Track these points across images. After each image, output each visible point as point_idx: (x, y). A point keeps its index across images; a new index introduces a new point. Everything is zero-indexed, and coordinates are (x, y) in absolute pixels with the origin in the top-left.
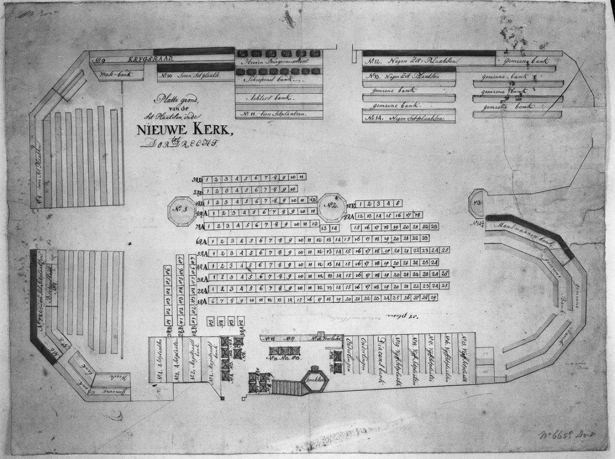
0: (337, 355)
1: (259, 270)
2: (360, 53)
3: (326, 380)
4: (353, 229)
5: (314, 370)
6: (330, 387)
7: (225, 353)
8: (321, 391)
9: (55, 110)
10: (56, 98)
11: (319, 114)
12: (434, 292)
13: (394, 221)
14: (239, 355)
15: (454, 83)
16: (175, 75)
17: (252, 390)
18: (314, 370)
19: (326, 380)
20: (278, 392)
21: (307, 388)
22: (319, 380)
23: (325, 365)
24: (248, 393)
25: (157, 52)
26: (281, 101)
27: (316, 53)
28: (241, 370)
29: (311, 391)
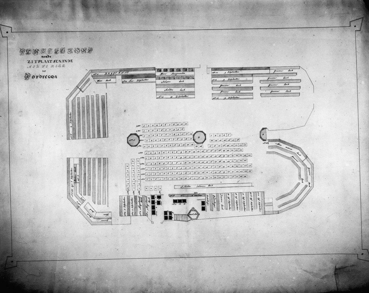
0: (203, 203)
1: (241, 168)
2: (210, 69)
3: (198, 214)
4: (209, 147)
5: (193, 209)
6: (199, 217)
7: (153, 202)
8: (196, 219)
9: (77, 96)
10: (78, 90)
11: (252, 97)
12: (245, 174)
13: (232, 143)
14: (159, 203)
15: (252, 82)
16: (135, 80)
17: (166, 218)
18: (193, 209)
19: (198, 214)
20: (184, 220)
21: (190, 217)
22: (196, 214)
23: (199, 208)
24: (164, 220)
25: (121, 70)
26: (288, 92)
27: (192, 70)
28: (160, 209)
29: (192, 219)
